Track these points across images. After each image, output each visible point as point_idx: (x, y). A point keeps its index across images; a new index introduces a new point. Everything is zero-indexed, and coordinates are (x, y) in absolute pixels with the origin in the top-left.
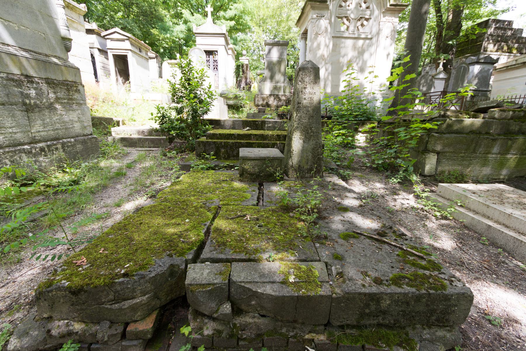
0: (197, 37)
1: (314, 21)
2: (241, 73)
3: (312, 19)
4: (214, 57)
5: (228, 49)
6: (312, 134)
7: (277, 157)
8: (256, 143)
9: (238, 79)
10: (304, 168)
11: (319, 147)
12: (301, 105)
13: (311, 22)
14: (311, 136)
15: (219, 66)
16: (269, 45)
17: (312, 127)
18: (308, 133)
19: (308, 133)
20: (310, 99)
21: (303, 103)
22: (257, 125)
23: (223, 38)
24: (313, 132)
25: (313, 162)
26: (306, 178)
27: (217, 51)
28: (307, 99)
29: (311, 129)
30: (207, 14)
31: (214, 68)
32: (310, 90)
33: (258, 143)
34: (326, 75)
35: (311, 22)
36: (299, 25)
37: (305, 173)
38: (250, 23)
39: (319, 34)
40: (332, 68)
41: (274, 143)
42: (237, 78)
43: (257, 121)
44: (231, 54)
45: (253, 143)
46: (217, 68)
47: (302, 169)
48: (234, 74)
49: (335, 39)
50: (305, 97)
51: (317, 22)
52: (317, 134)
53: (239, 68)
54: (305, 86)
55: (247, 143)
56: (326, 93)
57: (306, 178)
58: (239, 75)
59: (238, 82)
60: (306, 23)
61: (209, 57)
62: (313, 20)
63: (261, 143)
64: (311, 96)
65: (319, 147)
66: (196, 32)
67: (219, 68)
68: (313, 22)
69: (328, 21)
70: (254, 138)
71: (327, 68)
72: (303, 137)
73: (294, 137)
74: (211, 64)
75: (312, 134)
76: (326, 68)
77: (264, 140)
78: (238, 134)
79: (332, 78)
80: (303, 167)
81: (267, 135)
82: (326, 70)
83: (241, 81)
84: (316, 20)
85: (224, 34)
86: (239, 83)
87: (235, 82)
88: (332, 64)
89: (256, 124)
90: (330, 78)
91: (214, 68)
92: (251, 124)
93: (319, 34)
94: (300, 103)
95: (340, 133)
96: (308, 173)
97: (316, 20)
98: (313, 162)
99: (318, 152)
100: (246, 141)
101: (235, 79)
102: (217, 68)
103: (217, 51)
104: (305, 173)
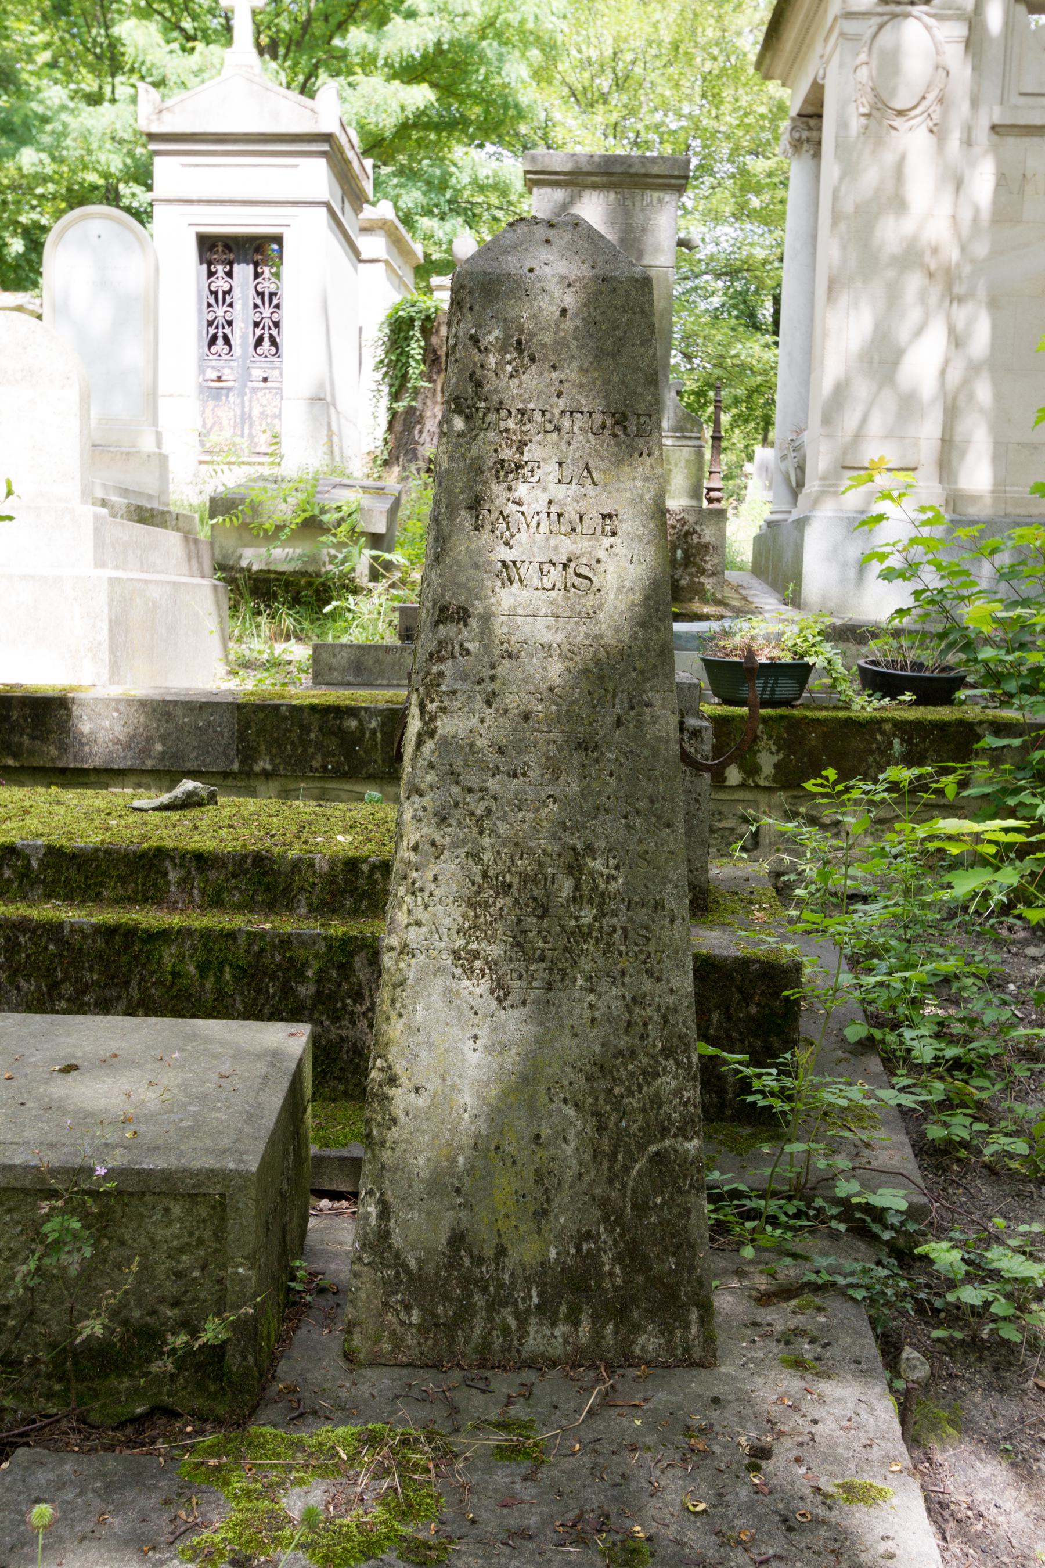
0: (157, 160)
1: (865, 28)
2: (415, 370)
3: (849, 15)
4: (257, 275)
5: (365, 230)
6: (587, 915)
7: (166, 1176)
8: (188, 932)
9: (401, 406)
10: (511, 1262)
11: (668, 1052)
12: (468, 636)
13: (842, 34)
14: (583, 934)
15: (285, 325)
16: (556, 184)
17: (590, 850)
18: (543, 911)
19: (543, 911)
20: (556, 574)
21: (486, 618)
22: (349, 742)
23: (322, 163)
24: (601, 900)
25: (603, 1203)
26: (530, 1364)
27: (278, 239)
28: (529, 573)
29: (574, 869)
30: (228, 28)
31: (259, 342)
32: (560, 492)
33: (206, 934)
34: (955, 376)
35: (842, 34)
36: (780, 67)
37: (522, 1320)
38: (527, 95)
39: (900, 113)
40: (994, 327)
41: (346, 940)
42: (395, 397)
43: (352, 712)
44: (384, 256)
45: (164, 935)
46: (273, 342)
47: (485, 1271)
48: (379, 376)
49: (1011, 141)
50: (507, 555)
51: (886, 38)
52: (642, 915)
53: (408, 339)
54: (507, 454)
55: (109, 932)
56: (955, 500)
57: (530, 1364)
58: (405, 377)
59: (398, 427)
60: (818, 48)
61: (229, 274)
62: (851, 27)
63: (231, 936)
64: (567, 546)
65: (668, 1052)
66: (155, 129)
67: (286, 339)
68: (856, 38)
69: (958, 30)
70: (183, 882)
71: (960, 325)
72: (495, 951)
73: (405, 950)
74: (242, 314)
75: (587, 915)
76: (951, 331)
77: (271, 907)
78: (52, 851)
79: (998, 396)
80: (501, 1252)
81: (296, 865)
82: (957, 340)
83: (421, 420)
84: (875, 21)
85: (327, 138)
86: (408, 427)
87: (384, 425)
88: (994, 304)
89: (341, 733)
90: (984, 392)
91: (259, 342)
92: (305, 729)
93: (900, 113)
94: (462, 615)
95: (977, 838)
96: (546, 1310)
97: (875, 21)
98: (603, 1203)
99: (657, 1102)
100: (109, 916)
101: (385, 402)
102: (273, 342)
103: (278, 239)
104: (522, 1320)
